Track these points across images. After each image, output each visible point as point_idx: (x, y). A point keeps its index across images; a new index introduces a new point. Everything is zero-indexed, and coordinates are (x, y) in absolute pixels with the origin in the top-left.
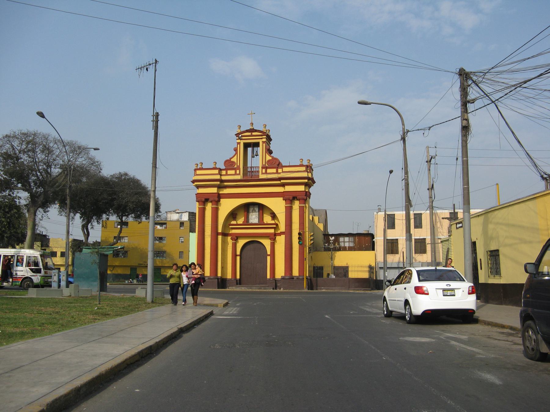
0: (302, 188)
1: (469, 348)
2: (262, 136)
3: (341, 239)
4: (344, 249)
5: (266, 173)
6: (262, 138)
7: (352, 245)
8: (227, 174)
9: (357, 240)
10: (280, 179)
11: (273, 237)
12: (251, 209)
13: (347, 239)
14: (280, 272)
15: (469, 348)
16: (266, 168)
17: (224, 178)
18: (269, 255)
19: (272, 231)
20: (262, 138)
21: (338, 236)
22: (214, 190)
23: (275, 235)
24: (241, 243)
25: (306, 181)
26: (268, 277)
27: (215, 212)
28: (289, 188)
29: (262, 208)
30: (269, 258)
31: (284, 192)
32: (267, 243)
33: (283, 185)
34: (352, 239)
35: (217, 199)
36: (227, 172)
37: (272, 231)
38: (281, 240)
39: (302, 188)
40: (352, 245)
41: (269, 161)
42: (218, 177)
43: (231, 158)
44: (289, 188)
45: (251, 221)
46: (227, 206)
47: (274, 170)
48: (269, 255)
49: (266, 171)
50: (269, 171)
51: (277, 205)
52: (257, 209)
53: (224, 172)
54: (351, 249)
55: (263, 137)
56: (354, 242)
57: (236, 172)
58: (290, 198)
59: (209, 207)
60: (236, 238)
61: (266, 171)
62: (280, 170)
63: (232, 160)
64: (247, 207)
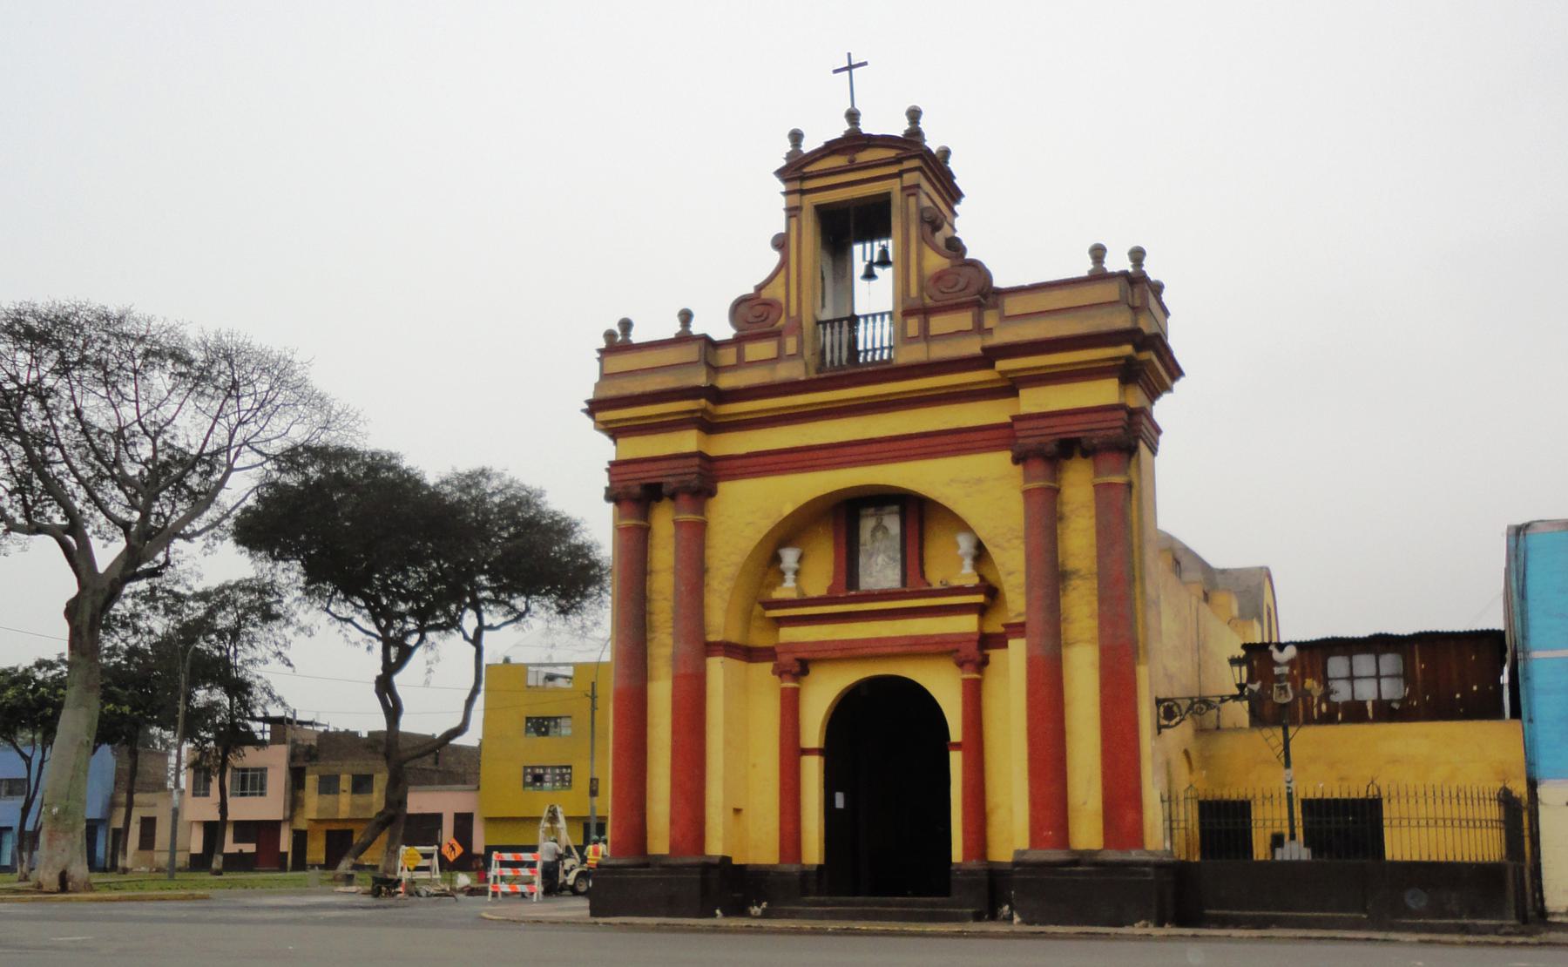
0: (1104, 392)
1: (1493, 922)
2: (898, 161)
3: (1337, 666)
4: (1355, 713)
5: (926, 336)
6: (899, 175)
7: (116, 606)
8: (741, 364)
9: (1420, 666)
10: (988, 357)
11: (975, 656)
12: (867, 525)
13: (1364, 664)
14: (1011, 834)
15: (1493, 922)
16: (925, 312)
17: (726, 382)
18: (957, 746)
19: (967, 624)
20: (899, 175)
21: (1317, 652)
22: (688, 441)
23: (989, 642)
24: (822, 693)
25: (1127, 349)
26: (957, 854)
27: (695, 538)
28: (1033, 401)
29: (919, 515)
30: (956, 759)
31: (1017, 418)
32: (943, 686)
33: (1009, 388)
34: (1390, 662)
35: (700, 482)
36: (740, 356)
37: (967, 624)
38: (1011, 667)
39: (1104, 392)
40: (1392, 690)
41: (939, 277)
42: (700, 379)
43: (759, 288)
44: (1033, 401)
45: (867, 582)
46: (747, 510)
47: (964, 320)
48: (957, 746)
49: (925, 328)
50: (939, 324)
51: (982, 492)
52: (893, 524)
53: (728, 357)
54: (1386, 712)
55: (907, 165)
56: (1407, 676)
57: (781, 347)
58: (1047, 450)
59: (664, 521)
60: (799, 666)
61: (925, 328)
62: (990, 319)
63: (765, 294)
64: (843, 515)
